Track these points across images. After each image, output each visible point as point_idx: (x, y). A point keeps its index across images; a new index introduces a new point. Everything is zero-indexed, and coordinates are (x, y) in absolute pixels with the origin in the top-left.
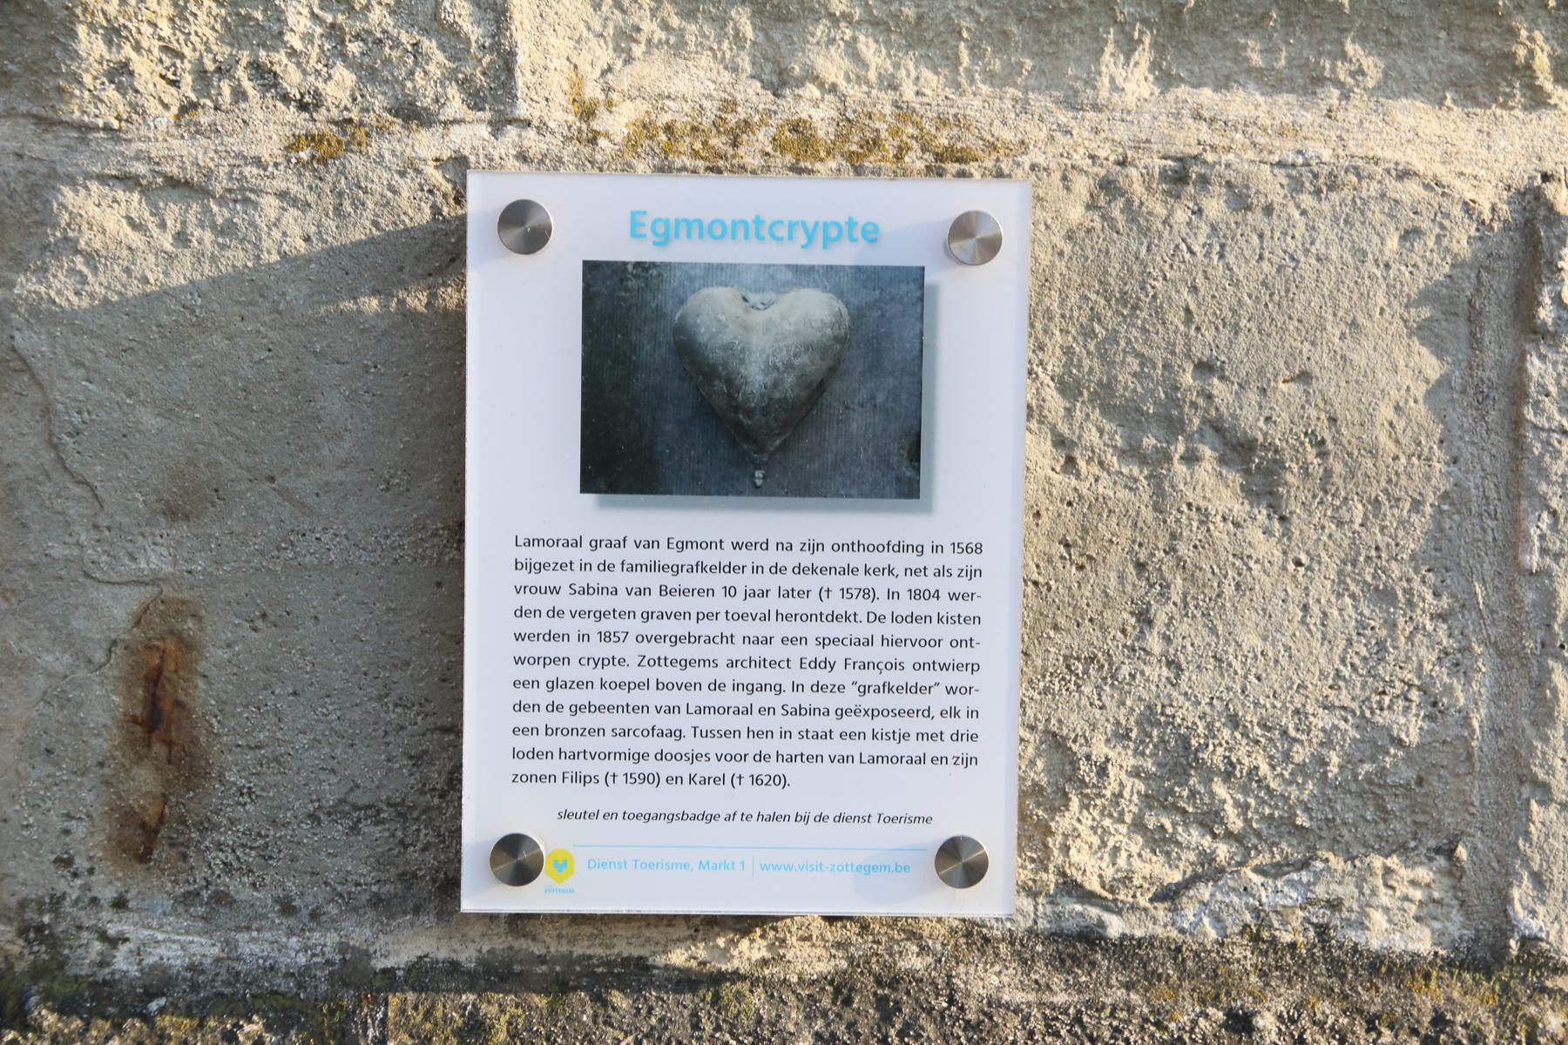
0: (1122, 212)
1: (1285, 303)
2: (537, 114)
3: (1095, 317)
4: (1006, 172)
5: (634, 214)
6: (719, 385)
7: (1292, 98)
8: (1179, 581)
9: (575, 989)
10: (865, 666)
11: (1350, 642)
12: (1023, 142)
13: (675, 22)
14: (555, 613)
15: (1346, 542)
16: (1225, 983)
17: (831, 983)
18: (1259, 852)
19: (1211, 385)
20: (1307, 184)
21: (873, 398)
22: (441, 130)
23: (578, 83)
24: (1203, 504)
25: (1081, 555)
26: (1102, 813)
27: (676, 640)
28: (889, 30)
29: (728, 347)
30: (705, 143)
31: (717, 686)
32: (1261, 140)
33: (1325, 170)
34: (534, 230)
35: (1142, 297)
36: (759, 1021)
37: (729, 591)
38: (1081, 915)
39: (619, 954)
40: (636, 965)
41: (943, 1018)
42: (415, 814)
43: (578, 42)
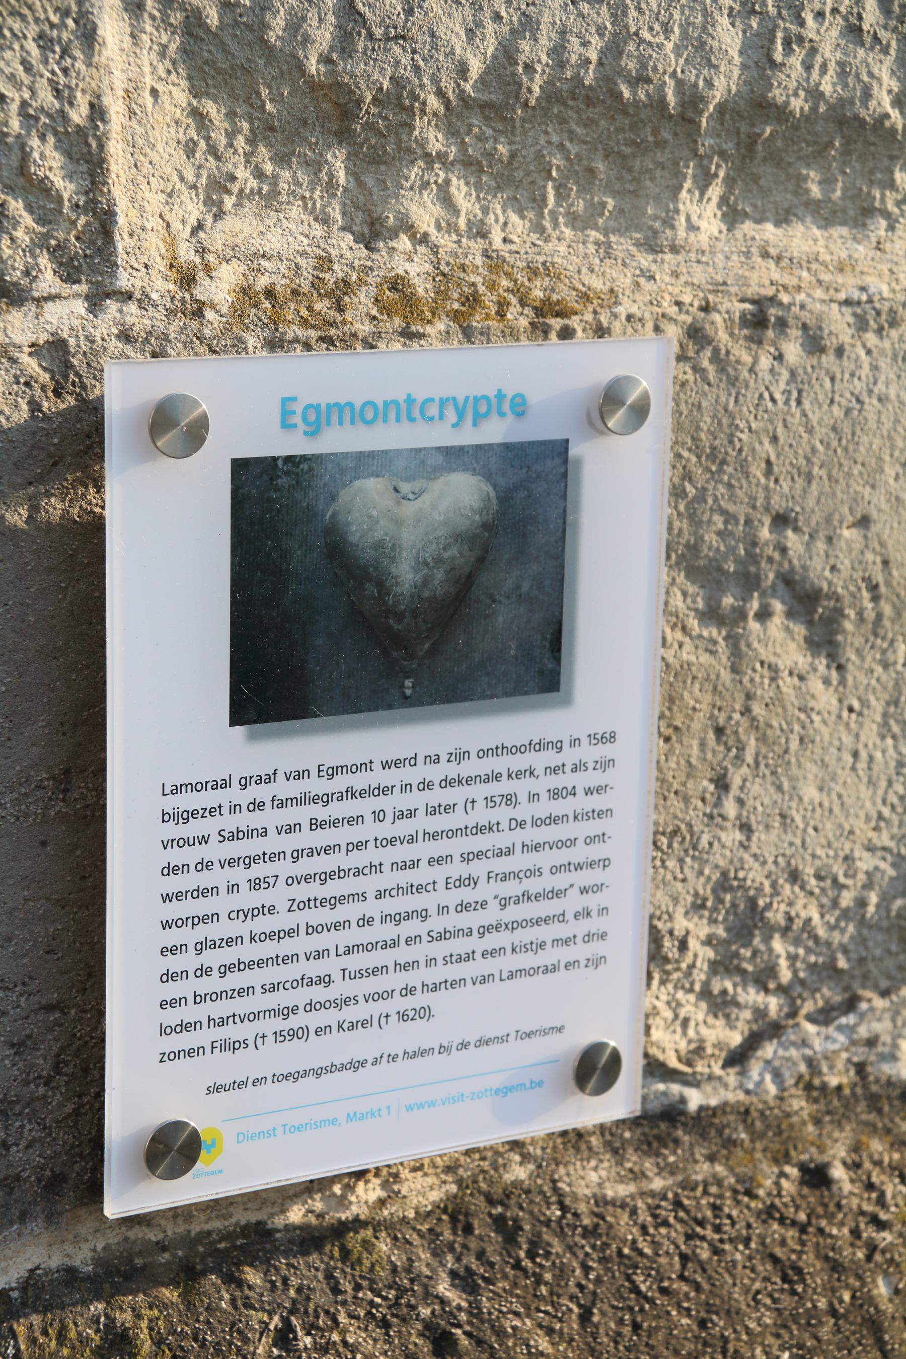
0: (711, 361)
1: (851, 447)
2: (138, 284)
3: (687, 476)
4: (605, 325)
5: (285, 401)
6: (371, 589)
7: (844, 231)
8: (753, 742)
9: (204, 1273)
10: (505, 878)
11: (890, 783)
12: (612, 291)
13: (269, 168)
14: (205, 865)
15: (891, 684)
16: (789, 1138)
17: (445, 1210)
18: (803, 1000)
19: (786, 537)
20: (872, 322)
21: (518, 587)
22: (33, 309)
23: (171, 243)
24: (773, 660)
25: (669, 726)
26: (676, 987)
27: (326, 877)
28: (481, 171)
29: (379, 546)
30: (310, 308)
31: (366, 921)
32: (826, 277)
33: (886, 307)
34: (190, 426)
35: (730, 450)
36: (394, 1270)
37: (379, 816)
38: (665, 1094)
39: (237, 1224)
40: (256, 1232)
41: (562, 1228)
42: (17, 1109)
43: (170, 195)
